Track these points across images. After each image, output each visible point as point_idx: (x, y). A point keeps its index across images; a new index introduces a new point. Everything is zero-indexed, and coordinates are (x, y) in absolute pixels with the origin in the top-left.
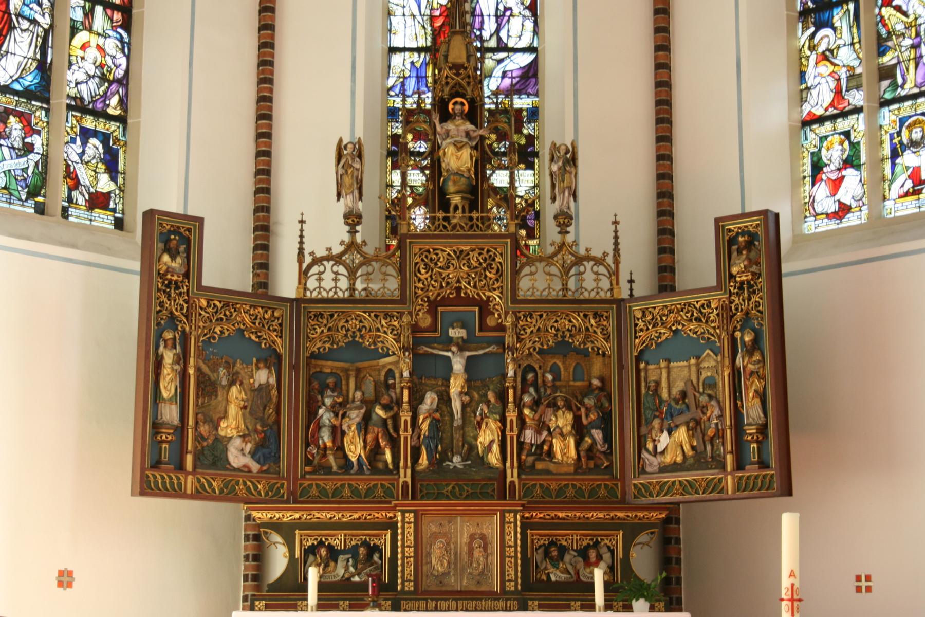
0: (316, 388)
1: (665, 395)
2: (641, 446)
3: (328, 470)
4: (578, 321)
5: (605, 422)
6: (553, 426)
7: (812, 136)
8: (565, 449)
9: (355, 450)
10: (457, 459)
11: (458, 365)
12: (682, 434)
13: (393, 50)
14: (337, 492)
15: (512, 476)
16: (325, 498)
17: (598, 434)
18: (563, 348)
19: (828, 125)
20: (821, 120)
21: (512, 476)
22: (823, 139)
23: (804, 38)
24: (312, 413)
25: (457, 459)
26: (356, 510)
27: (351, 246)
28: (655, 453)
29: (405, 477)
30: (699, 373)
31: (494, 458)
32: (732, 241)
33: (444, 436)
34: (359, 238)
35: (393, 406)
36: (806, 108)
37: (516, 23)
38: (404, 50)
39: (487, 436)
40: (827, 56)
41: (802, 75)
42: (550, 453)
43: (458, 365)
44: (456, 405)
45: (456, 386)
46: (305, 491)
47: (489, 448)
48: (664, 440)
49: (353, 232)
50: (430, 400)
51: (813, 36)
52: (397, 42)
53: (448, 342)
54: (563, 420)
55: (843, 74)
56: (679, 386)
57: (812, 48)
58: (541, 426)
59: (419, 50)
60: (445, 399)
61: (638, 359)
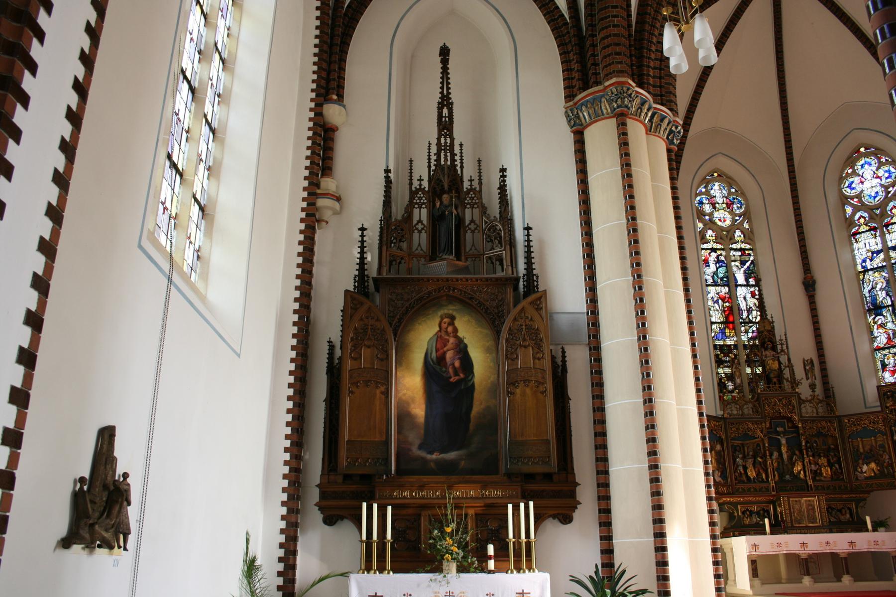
0: (735, 449)
1: (862, 451)
2: (855, 470)
3: (743, 482)
4: (824, 424)
5: (839, 462)
6: (820, 463)
7: (879, 355)
8: (826, 472)
9: (752, 473)
10: (787, 477)
11: (783, 441)
12: (873, 465)
13: (712, 323)
14: (749, 490)
15: (810, 482)
16: (744, 492)
17: (837, 466)
18: (819, 434)
19: (886, 351)
20: (883, 349)
21: (810, 482)
22: (885, 355)
23: (870, 319)
24: (734, 461)
25: (787, 477)
26: (423, 498)
27: (813, 397)
28: (862, 472)
29: (772, 484)
30: (876, 442)
31: (802, 475)
32: (885, 394)
33: (784, 469)
34: (816, 393)
35: (764, 456)
36: (875, 345)
37: (754, 313)
38: (716, 323)
39: (798, 468)
40: (882, 326)
41: (872, 333)
42: (821, 474)
43: (783, 441)
44: (785, 456)
45: (784, 450)
46: (738, 490)
47: (799, 472)
48: (865, 468)
49: (813, 391)
50: (775, 454)
51: (874, 319)
52: (713, 320)
53: (778, 433)
54: (823, 461)
55: (891, 332)
56: (867, 448)
57: (875, 323)
58: (816, 464)
59: (721, 323)
60: (781, 454)
61: (849, 438)
